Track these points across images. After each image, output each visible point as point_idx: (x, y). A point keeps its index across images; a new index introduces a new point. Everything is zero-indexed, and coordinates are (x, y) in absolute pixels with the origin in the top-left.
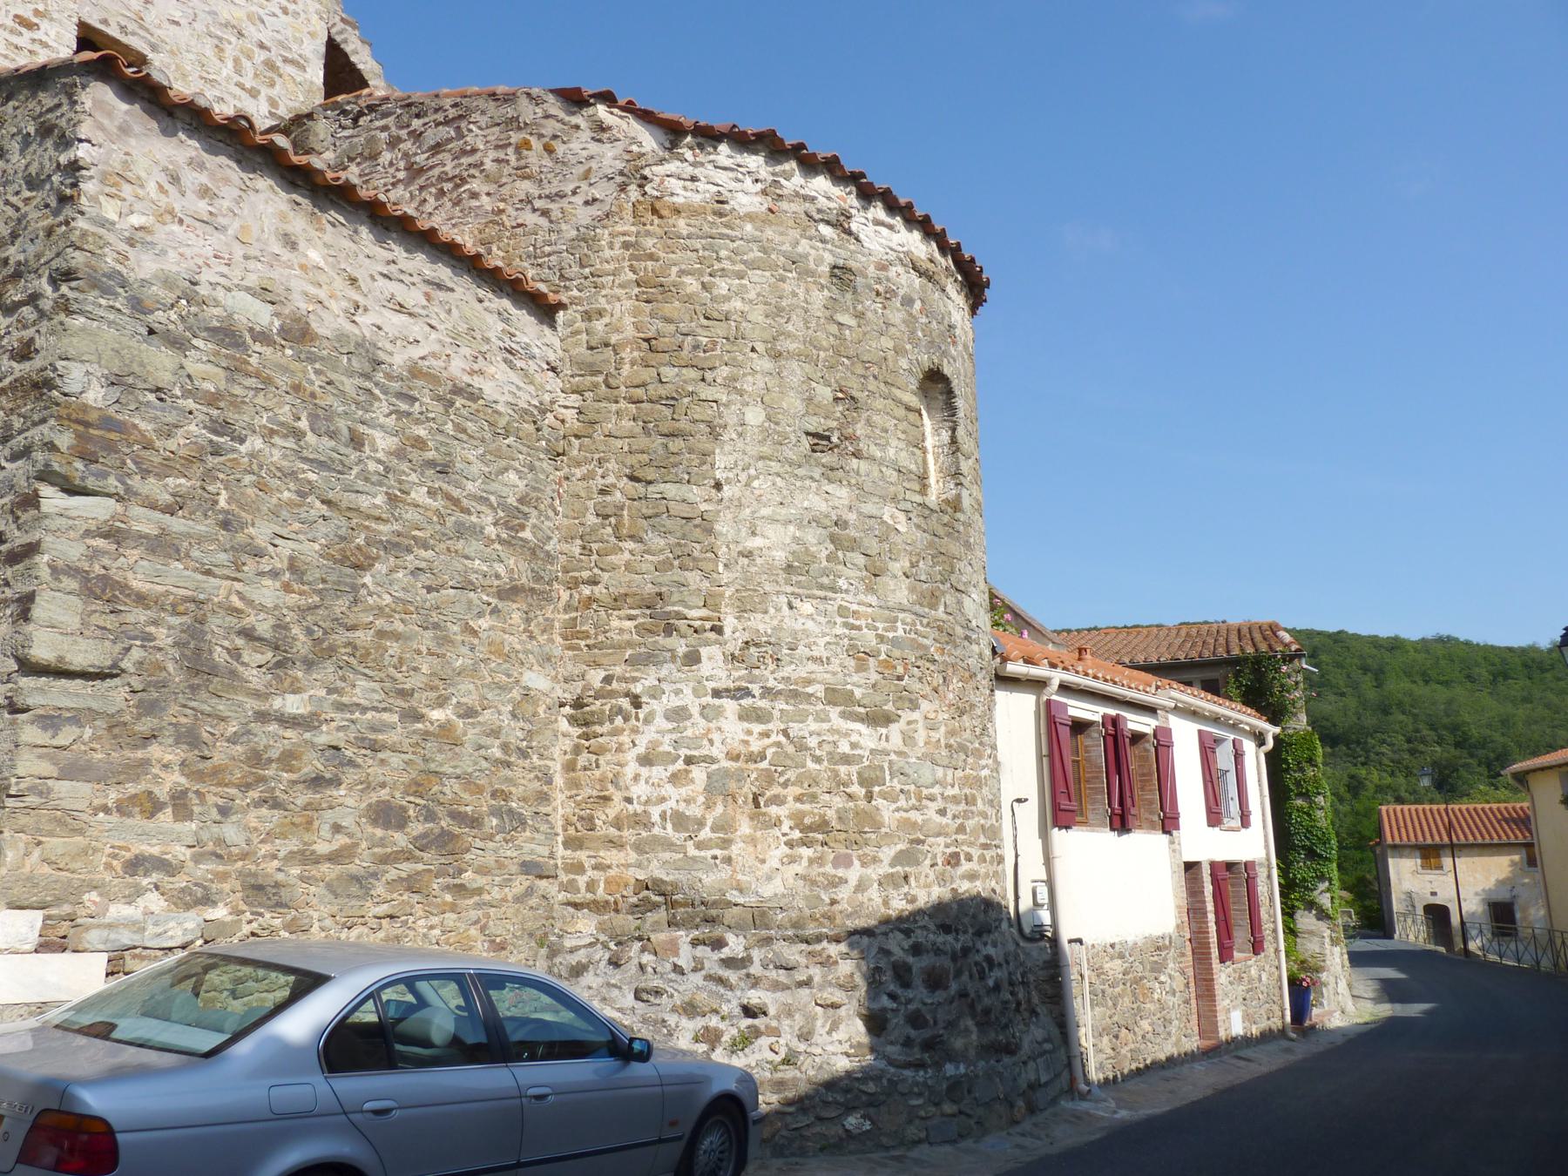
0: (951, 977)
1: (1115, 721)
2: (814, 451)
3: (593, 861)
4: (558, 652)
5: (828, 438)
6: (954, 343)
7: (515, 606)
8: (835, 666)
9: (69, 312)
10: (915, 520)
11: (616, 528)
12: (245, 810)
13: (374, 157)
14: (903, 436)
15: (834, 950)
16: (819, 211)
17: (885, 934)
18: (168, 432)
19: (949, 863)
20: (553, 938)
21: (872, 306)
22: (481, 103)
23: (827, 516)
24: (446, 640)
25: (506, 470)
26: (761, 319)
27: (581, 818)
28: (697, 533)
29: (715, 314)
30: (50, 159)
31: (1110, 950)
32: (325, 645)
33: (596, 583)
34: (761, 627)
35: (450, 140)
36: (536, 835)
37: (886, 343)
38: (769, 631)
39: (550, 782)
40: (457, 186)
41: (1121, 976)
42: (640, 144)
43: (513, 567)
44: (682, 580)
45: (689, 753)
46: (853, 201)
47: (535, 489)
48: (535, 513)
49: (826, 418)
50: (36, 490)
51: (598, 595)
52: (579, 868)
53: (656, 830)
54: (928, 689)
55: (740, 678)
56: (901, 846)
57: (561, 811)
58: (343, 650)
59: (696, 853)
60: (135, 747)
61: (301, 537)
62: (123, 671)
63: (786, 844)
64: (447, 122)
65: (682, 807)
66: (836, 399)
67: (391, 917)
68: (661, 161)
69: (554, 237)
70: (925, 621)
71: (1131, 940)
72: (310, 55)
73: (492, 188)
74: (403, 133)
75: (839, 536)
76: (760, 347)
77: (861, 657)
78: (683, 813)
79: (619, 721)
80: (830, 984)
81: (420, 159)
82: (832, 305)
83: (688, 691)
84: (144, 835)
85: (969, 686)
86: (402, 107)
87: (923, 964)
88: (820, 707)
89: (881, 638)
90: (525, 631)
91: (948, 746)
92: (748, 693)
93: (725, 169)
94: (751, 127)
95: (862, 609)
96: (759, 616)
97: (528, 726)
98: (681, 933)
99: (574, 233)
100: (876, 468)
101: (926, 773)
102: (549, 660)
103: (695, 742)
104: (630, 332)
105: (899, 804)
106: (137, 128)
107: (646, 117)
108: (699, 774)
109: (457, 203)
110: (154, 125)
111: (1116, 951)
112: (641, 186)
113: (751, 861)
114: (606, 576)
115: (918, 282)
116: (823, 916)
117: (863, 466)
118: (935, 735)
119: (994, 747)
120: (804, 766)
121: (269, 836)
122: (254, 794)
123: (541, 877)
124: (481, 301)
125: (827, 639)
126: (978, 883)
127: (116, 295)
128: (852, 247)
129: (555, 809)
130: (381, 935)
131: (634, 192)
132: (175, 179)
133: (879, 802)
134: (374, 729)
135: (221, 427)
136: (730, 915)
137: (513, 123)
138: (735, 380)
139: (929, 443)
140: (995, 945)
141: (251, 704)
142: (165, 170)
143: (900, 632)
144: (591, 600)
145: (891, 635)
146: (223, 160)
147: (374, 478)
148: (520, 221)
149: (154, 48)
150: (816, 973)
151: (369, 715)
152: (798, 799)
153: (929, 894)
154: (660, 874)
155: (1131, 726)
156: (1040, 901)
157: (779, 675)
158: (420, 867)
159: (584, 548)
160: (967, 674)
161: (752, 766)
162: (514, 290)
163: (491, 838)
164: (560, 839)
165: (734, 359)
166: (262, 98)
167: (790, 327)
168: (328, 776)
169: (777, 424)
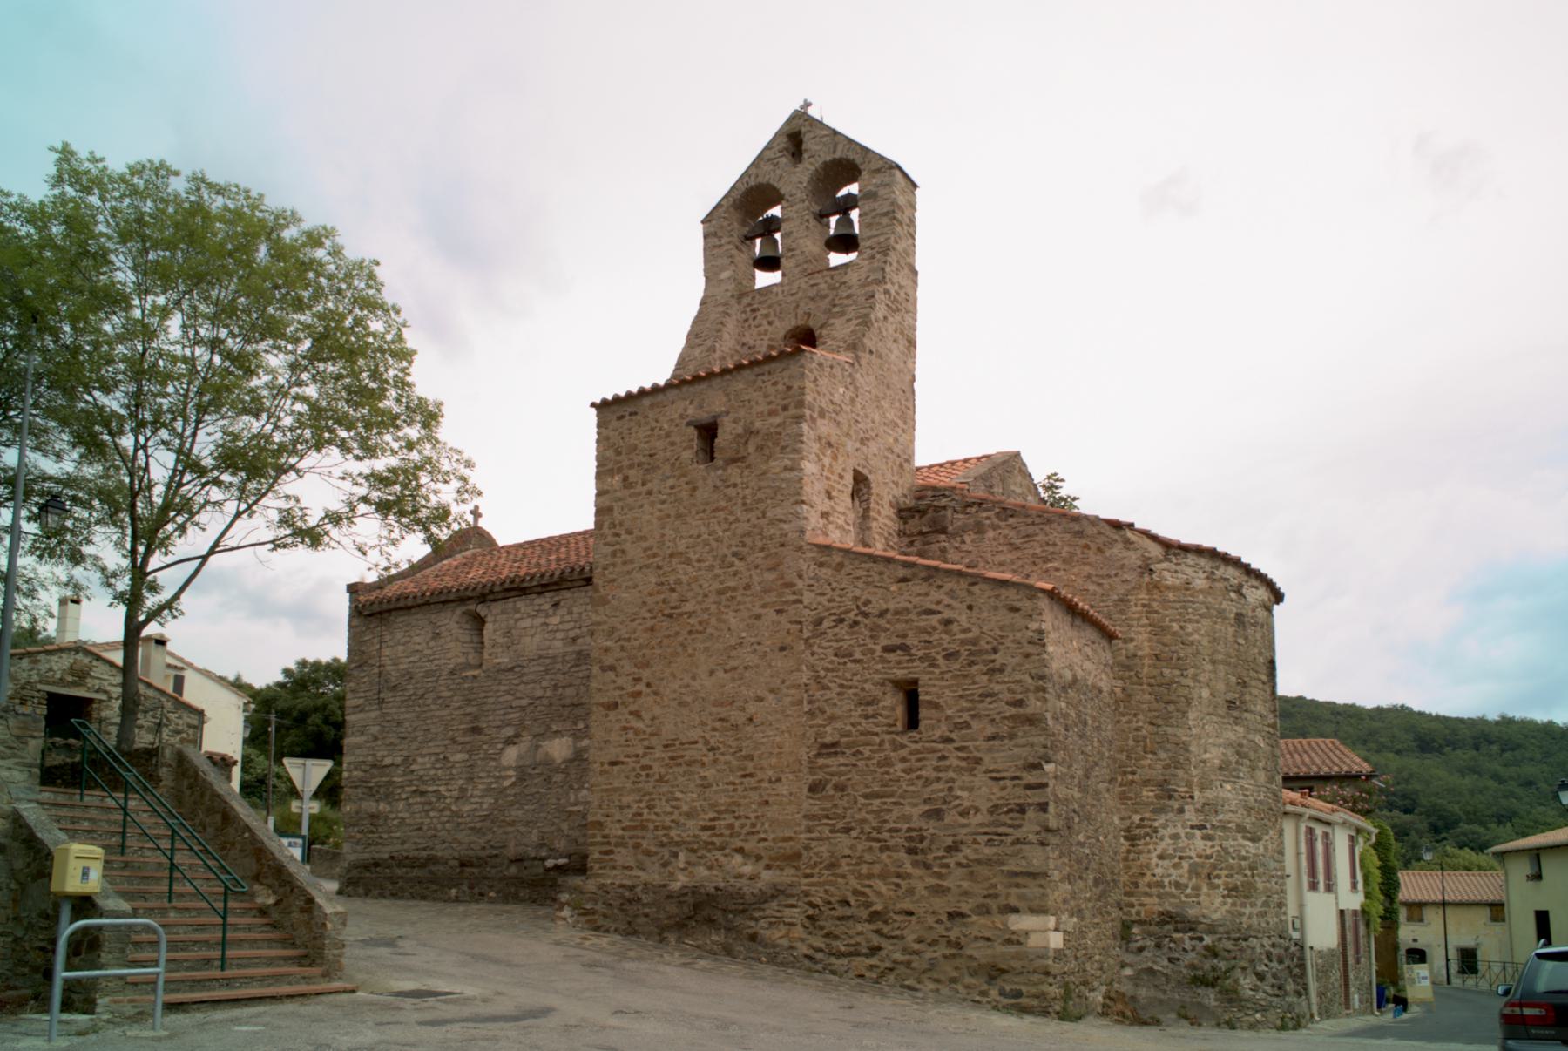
28: (1182, 751)
37: (1256, 651)
52: (1132, 906)
53: (1167, 889)
68: (1160, 562)
76: (1207, 658)
77: (1249, 809)
103: (1183, 850)
108: (1185, 864)
152: (1227, 876)
154: (1170, 909)
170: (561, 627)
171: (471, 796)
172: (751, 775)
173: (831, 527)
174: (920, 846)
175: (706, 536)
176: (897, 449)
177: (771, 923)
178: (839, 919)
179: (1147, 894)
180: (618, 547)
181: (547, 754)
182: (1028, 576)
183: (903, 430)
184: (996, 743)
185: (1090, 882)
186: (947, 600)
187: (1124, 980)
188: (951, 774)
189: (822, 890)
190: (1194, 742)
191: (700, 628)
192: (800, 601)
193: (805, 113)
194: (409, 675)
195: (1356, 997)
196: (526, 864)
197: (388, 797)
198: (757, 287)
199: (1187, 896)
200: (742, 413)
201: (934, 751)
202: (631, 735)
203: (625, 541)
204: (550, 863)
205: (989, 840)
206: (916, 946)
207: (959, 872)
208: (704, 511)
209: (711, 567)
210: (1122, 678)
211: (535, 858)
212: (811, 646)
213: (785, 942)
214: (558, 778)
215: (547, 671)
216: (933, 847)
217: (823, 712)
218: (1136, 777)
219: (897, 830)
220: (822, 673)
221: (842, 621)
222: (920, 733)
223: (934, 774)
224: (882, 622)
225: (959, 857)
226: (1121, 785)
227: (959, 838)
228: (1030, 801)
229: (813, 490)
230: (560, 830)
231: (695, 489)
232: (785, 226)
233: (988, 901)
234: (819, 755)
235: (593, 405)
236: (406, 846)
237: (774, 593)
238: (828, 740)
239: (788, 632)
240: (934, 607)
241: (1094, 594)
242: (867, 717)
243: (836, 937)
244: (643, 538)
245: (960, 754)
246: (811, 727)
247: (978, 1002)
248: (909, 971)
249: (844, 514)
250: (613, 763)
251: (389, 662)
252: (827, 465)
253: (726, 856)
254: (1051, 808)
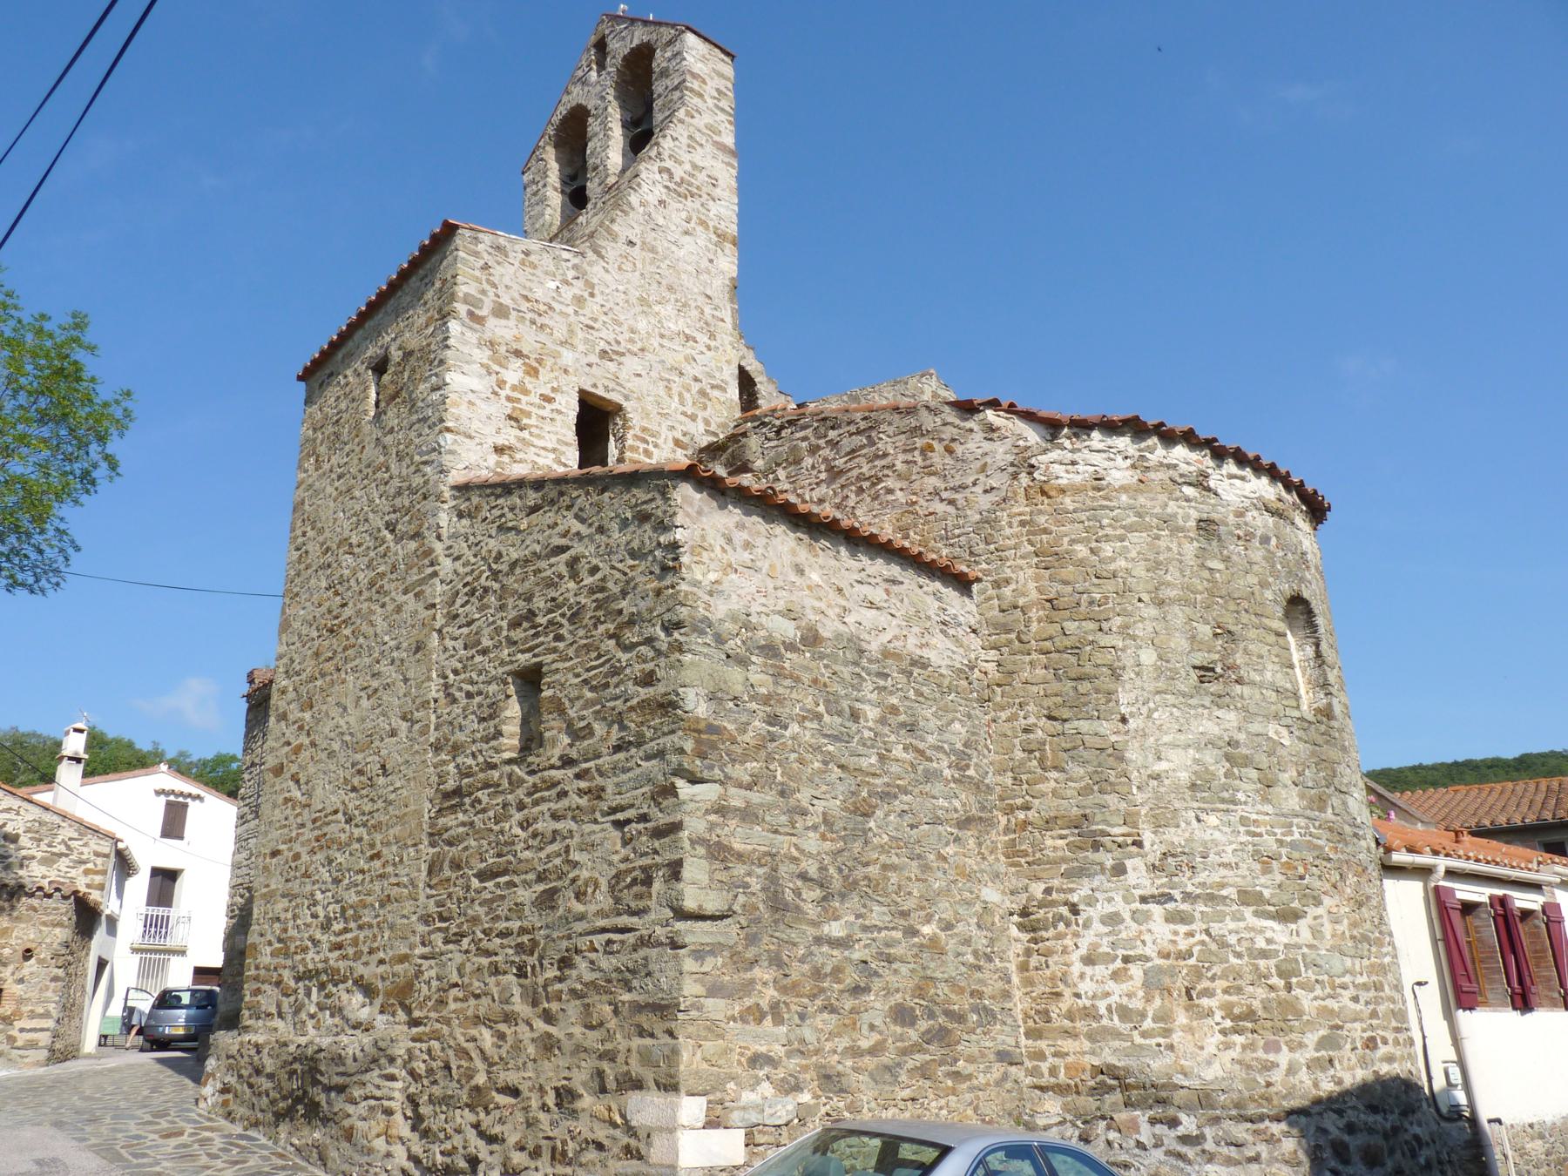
0: (1386, 1154)
1: (1503, 901)
2: (1202, 682)
3: (1052, 1049)
4: (1003, 869)
5: (1213, 670)
6: (1308, 567)
7: (969, 833)
8: (1243, 871)
9: (681, 651)
10: (1297, 733)
11: (1041, 761)
12: (814, 1016)
13: (797, 462)
14: (1276, 660)
15: (1277, 1128)
16: (1181, 476)
17: (1320, 1114)
18: (743, 729)
19: (1368, 1047)
20: (1026, 1118)
21: (1235, 549)
22: (887, 416)
23: (1220, 738)
24: (926, 868)
25: (953, 721)
26: (1143, 573)
27: (1038, 1012)
29: (1105, 574)
30: (650, 538)
31: (1529, 1130)
32: (851, 880)
33: (1028, 809)
34: (1176, 840)
35: (863, 447)
36: (1005, 1028)
37: (1252, 579)
38: (1183, 843)
39: (1009, 982)
40: (874, 484)
41: (1543, 1157)
42: (1026, 439)
43: (964, 801)
44: (1103, 803)
45: (1125, 953)
46: (1209, 462)
47: (974, 734)
48: (975, 753)
49: (1209, 652)
50: (673, 784)
51: (1031, 819)
52: (1040, 1056)
53: (1105, 1022)
54: (1328, 886)
55: (1163, 885)
56: (1322, 1032)
57: (1020, 1006)
58: (862, 883)
59: (1142, 1041)
60: (746, 970)
61: (828, 796)
62: (734, 912)
63: (1220, 1032)
64: (859, 432)
65: (1125, 1001)
66: (1216, 635)
67: (913, 1100)
68: (1045, 451)
69: (961, 521)
70: (1317, 824)
71: (1549, 1119)
72: (728, 378)
73: (904, 484)
74: (822, 442)
75: (1233, 756)
76: (1145, 597)
77: (1266, 861)
78: (1126, 1007)
79: (1061, 926)
80: (1277, 1160)
81: (840, 462)
82: (1202, 554)
83: (1118, 898)
84: (757, 1037)
85: (1363, 880)
86: (817, 421)
87: (1359, 1142)
88: (1235, 907)
89: (1281, 843)
90: (979, 853)
91: (1353, 937)
92: (1171, 898)
93: (1099, 451)
94: (1117, 415)
95: (1261, 817)
96: (1173, 830)
97: (989, 935)
98: (1138, 1113)
99: (978, 517)
100: (1257, 691)
101: (1337, 963)
102: (998, 876)
104: (1034, 595)
105: (1316, 993)
106: (706, 509)
107: (1029, 416)
108: (1136, 970)
109: (875, 498)
110: (715, 504)
111: (1534, 1130)
112: (1030, 473)
113: (1191, 1048)
114: (1036, 802)
115: (1271, 520)
116: (1261, 1097)
117: (1246, 690)
118: (1340, 928)
119: (1391, 935)
120: (1227, 962)
121: (832, 1035)
122: (819, 1002)
123: (1011, 1064)
124: (921, 587)
125: (1234, 846)
126: (1396, 1065)
127: (706, 633)
128: (1212, 501)
129: (1015, 1005)
130: (907, 1115)
131: (1024, 479)
132: (729, 540)
133: (1297, 992)
134: (888, 945)
135: (773, 720)
136: (1179, 1096)
137: (917, 431)
138: (1128, 628)
139: (1296, 657)
140: (1420, 1125)
141: (811, 931)
142: (724, 535)
143: (1297, 836)
144: (1026, 823)
145: (1289, 839)
146: (755, 518)
147: (869, 743)
148: (931, 510)
149: (627, 398)
150: (1263, 1149)
151: (883, 933)
152: (1226, 991)
153: (1354, 1077)
155: (1519, 904)
156: (1453, 1082)
157: (1196, 880)
158: (928, 1057)
159: (1015, 779)
160: (1360, 869)
161: (1182, 963)
162: (943, 574)
163: (973, 1031)
164: (1022, 1030)
165: (1125, 610)
166: (699, 420)
167: (1169, 578)
168: (862, 985)
169: (1168, 661)
179: (1069, 1034)
199: (1144, 1035)
201: (554, 785)
205: (609, 942)
218: (1032, 814)
226: (1007, 830)
228: (658, 859)
240: (563, 542)
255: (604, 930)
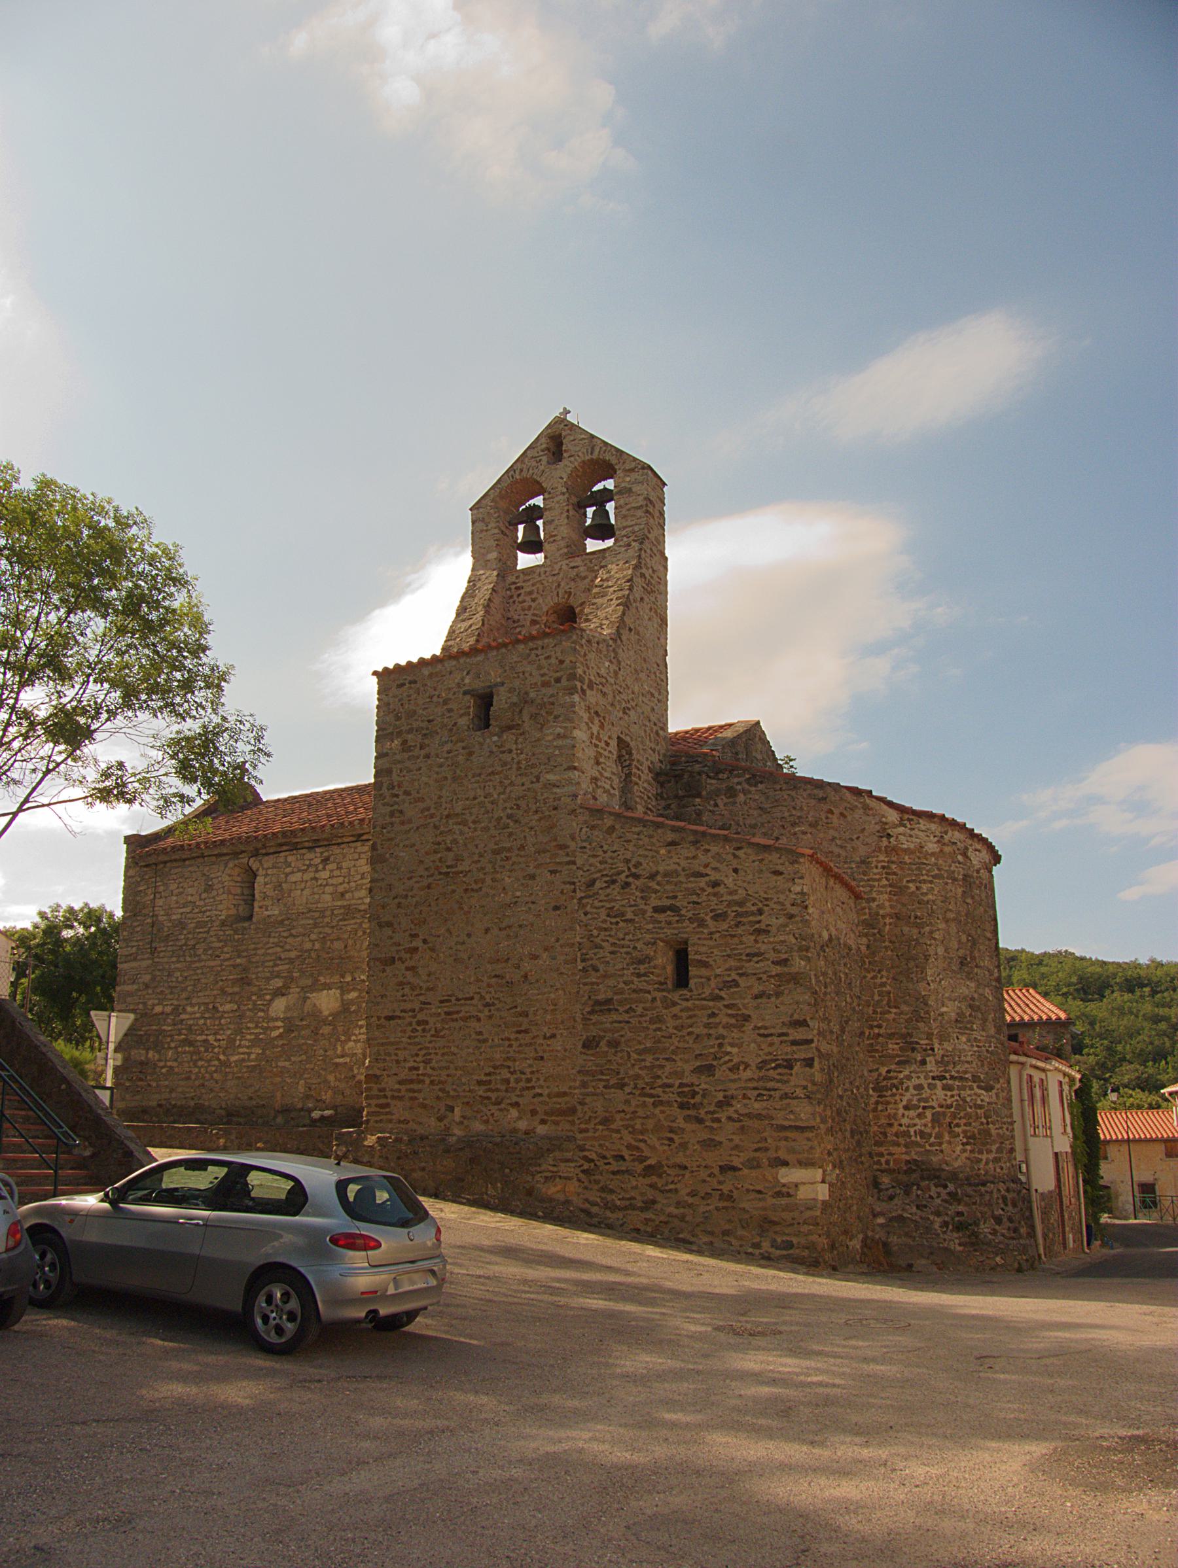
8: (974, 1065)
52: (882, 1155)
53: (913, 1138)
65: (923, 1128)
68: (896, 826)
76: (940, 917)
83: (922, 1077)
92: (945, 1078)
103: (926, 1100)
154: (916, 1157)
170: (331, 881)
171: (240, 1046)
172: (526, 1031)
173: (599, 791)
174: (692, 1101)
175: (482, 798)
176: (653, 719)
177: (546, 1178)
178: (614, 1173)
180: (396, 807)
181: (315, 1005)
182: (777, 839)
183: (659, 701)
184: (764, 1000)
185: (848, 1134)
186: (714, 864)
187: (878, 1229)
188: (721, 1031)
189: (596, 1144)
190: (933, 997)
191: (475, 887)
192: (574, 863)
193: (565, 419)
194: (181, 925)
195: (1071, 1236)
196: (293, 1115)
197: (158, 1046)
198: (519, 568)
200: (517, 683)
201: (703, 1008)
202: (407, 990)
203: (404, 801)
204: (316, 1114)
206: (690, 1200)
207: (730, 1127)
208: (480, 775)
209: (486, 829)
210: (866, 935)
211: (302, 1109)
212: (584, 906)
213: (561, 1197)
214: (326, 1030)
215: (316, 925)
216: (705, 1101)
217: (597, 970)
219: (670, 1086)
220: (595, 932)
221: (614, 882)
222: (691, 991)
223: (705, 1031)
224: (653, 884)
225: (730, 1112)
226: (868, 1039)
227: (729, 1093)
228: (796, 1056)
229: (585, 755)
230: (326, 1081)
231: (470, 754)
232: (546, 514)
233: (757, 1154)
234: (592, 1012)
235: (375, 673)
236: (174, 1095)
237: (548, 854)
238: (601, 997)
239: (562, 892)
240: (704, 871)
241: (839, 856)
242: (639, 975)
243: (612, 1191)
244: (422, 800)
245: (730, 1012)
246: (585, 984)
247: (751, 1254)
248: (683, 1224)
249: (610, 779)
250: (389, 1018)
251: (162, 913)
252: (596, 733)
253: (501, 1110)
254: (816, 1063)
255: (755, 1088)
